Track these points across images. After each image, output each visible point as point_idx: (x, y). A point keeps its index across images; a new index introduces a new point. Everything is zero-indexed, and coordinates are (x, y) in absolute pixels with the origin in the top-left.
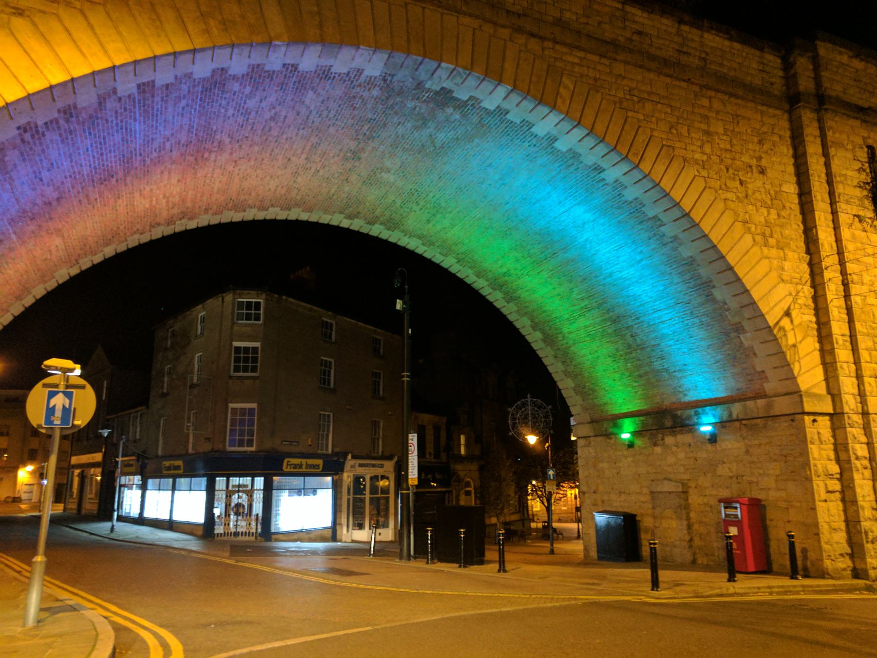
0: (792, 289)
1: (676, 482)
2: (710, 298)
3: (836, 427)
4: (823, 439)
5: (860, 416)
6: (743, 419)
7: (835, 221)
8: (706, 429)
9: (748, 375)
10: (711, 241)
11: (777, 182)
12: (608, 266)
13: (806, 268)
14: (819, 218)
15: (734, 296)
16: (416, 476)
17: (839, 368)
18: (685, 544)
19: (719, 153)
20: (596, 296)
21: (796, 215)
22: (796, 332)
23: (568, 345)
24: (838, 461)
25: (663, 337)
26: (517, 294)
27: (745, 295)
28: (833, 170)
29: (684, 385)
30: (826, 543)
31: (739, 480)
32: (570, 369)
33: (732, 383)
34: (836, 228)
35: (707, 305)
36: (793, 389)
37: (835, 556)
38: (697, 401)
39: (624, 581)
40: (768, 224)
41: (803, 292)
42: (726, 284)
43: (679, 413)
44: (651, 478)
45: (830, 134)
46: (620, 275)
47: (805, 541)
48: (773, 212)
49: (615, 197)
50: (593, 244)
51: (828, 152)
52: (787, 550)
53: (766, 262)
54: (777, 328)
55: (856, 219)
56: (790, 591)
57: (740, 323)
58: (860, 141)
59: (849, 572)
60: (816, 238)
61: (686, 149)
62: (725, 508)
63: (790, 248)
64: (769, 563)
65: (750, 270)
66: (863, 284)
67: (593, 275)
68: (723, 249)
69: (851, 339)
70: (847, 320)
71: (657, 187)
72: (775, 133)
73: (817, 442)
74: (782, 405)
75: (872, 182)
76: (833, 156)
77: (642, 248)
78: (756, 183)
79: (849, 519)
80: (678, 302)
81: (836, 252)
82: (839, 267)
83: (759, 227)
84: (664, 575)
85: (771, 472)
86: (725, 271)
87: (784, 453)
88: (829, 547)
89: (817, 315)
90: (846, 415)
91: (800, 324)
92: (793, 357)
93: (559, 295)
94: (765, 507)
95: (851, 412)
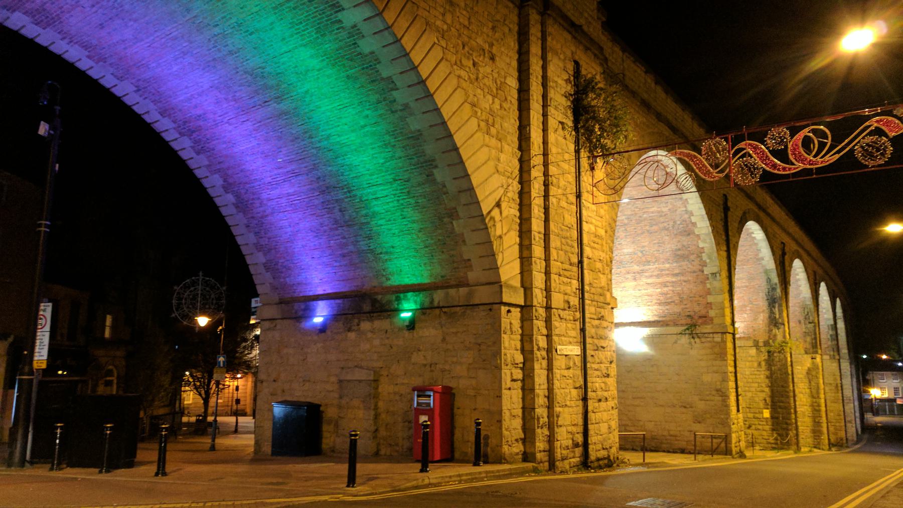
0: (504, 181)
1: (368, 369)
4: (514, 329)
5: (544, 309)
12: (327, 127)
14: (533, 117)
15: (455, 179)
16: (45, 357)
19: (458, 27)
20: (307, 160)
21: (514, 110)
24: (523, 351)
25: (374, 214)
28: (548, 75)
29: (388, 268)
30: (506, 430)
31: (432, 368)
32: (263, 242)
33: (438, 270)
34: (545, 130)
37: (511, 441)
40: (491, 113)
41: (513, 186)
43: (379, 297)
44: (342, 366)
45: (549, 39)
46: (338, 139)
49: (350, 46)
50: (314, 97)
52: (472, 438)
53: (485, 149)
56: (476, 478)
57: (455, 208)
58: (569, 53)
61: (429, 12)
62: (419, 396)
63: (506, 141)
65: (473, 154)
66: (559, 187)
69: (545, 237)
70: (543, 219)
73: (509, 332)
74: (482, 295)
75: (574, 94)
78: (486, 69)
79: (526, 406)
80: (397, 178)
83: (484, 113)
84: (362, 468)
87: (479, 341)
89: (520, 210)
91: (507, 217)
92: (498, 247)
94: (454, 394)
95: (538, 305)
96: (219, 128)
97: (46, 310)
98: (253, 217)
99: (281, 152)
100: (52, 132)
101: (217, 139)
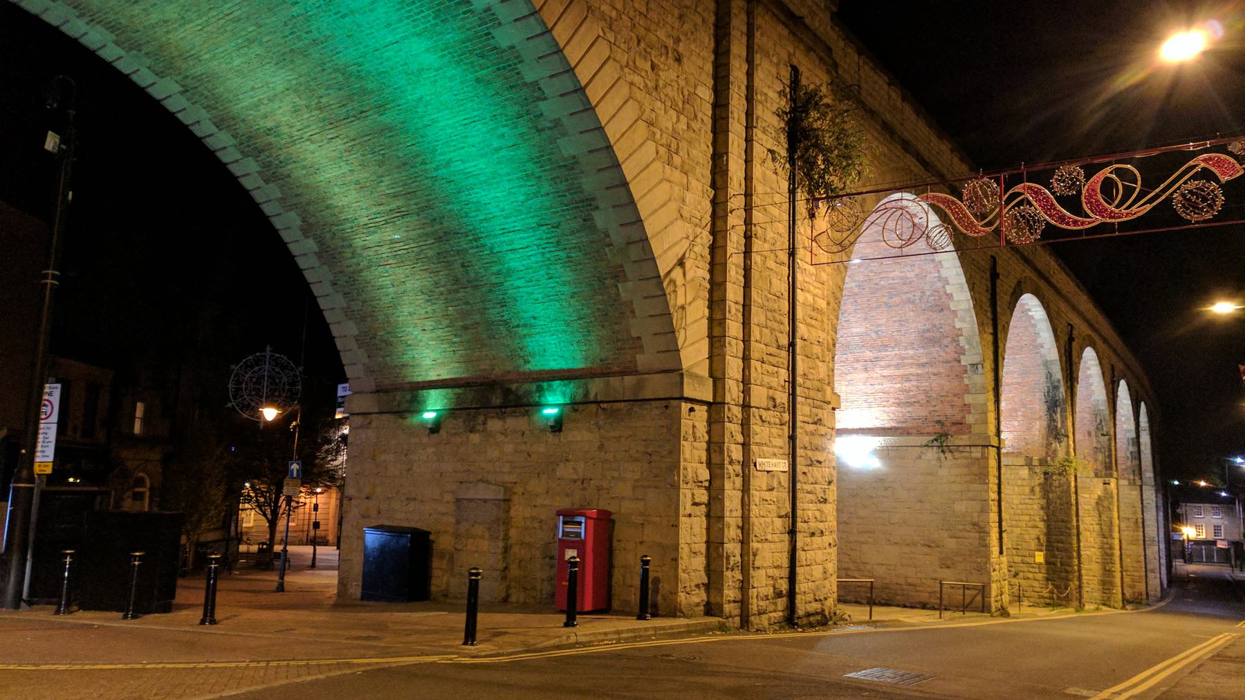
0: (690, 231)
2: (588, 224)
3: (712, 420)
4: (698, 435)
7: (749, 150)
8: (550, 412)
10: (606, 139)
12: (446, 150)
13: (708, 207)
15: (622, 225)
18: (496, 574)
19: (632, 14)
23: (360, 268)
24: (709, 464)
25: (510, 272)
26: (285, 171)
30: (684, 571)
31: (585, 485)
34: (748, 161)
35: (583, 234)
37: (690, 587)
38: (541, 372)
39: (417, 632)
43: (514, 387)
45: (758, 34)
47: (659, 569)
48: (683, 119)
49: (481, 36)
50: (429, 107)
51: (753, 58)
52: (637, 581)
53: (666, 185)
54: (667, 280)
55: (770, 155)
57: (622, 266)
58: (785, 57)
59: (702, 608)
60: (725, 168)
62: (565, 523)
67: (419, 160)
71: (548, 34)
72: (699, 13)
73: (691, 438)
74: (656, 386)
75: (790, 112)
76: (757, 65)
77: (505, 130)
80: (542, 222)
81: (743, 193)
83: (664, 135)
85: (629, 475)
86: (617, 186)
87: (650, 450)
89: (711, 272)
92: (679, 323)
93: (358, 182)
94: (613, 522)
95: (732, 402)
96: (298, 146)
97: (53, 394)
98: (341, 272)
99: (382, 182)
100: (64, 147)
101: (295, 162)
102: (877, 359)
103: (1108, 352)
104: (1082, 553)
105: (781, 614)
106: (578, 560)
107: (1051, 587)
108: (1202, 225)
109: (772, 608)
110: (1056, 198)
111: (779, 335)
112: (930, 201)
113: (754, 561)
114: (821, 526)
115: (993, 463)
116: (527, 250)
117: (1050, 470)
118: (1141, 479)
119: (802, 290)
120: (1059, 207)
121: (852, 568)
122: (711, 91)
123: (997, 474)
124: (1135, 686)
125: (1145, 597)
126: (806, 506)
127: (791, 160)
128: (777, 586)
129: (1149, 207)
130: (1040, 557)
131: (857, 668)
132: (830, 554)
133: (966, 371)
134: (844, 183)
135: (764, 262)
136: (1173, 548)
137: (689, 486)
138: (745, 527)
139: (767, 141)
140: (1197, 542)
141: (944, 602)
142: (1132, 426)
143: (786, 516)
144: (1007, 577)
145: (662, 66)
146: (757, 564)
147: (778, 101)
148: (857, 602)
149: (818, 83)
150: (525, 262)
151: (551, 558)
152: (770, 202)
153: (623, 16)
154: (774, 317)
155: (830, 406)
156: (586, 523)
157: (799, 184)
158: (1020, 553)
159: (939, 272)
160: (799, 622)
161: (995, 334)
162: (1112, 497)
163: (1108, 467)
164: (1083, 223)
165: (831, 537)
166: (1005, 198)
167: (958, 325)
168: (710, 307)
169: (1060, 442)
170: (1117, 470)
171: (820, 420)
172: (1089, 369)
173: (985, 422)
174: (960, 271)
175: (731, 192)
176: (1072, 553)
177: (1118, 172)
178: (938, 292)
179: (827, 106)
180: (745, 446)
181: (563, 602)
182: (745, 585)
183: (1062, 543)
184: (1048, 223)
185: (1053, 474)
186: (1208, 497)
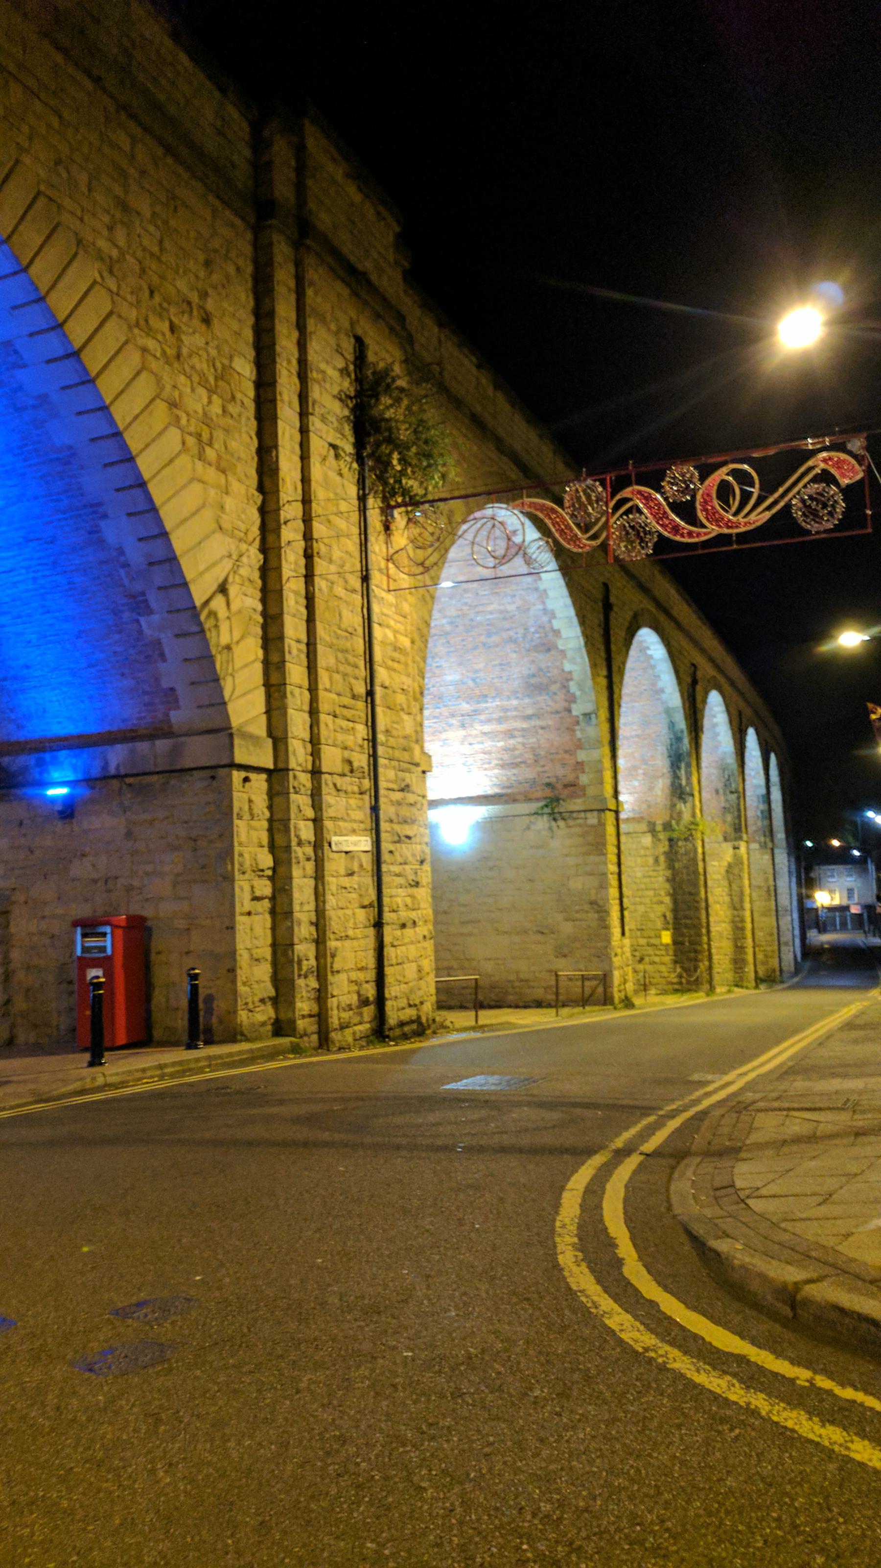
0: (233, 547)
4: (256, 811)
6: (127, 776)
9: (145, 693)
10: (112, 422)
11: (226, 349)
17: (288, 695)
19: (139, 254)
21: (248, 419)
22: (234, 625)
24: (272, 847)
27: (159, 541)
28: (310, 358)
30: (244, 984)
34: (305, 457)
36: (217, 724)
38: (42, 741)
41: (249, 557)
42: (129, 515)
45: (310, 292)
52: (184, 1002)
53: (197, 487)
55: (332, 452)
56: (190, 1070)
57: (143, 594)
58: (346, 324)
59: (269, 1028)
62: (84, 935)
63: (235, 474)
64: (148, 1027)
65: (174, 495)
68: (134, 442)
70: (305, 617)
71: (23, 275)
73: (247, 816)
75: (355, 397)
76: (311, 333)
80: (31, 536)
81: (300, 498)
82: (301, 526)
83: (193, 421)
85: (166, 869)
86: (131, 487)
87: (194, 834)
88: (247, 989)
89: (264, 601)
90: (291, 773)
91: (240, 612)
94: (149, 930)
95: (299, 768)
102: (476, 712)
103: (735, 697)
104: (712, 929)
105: (368, 1026)
106: (103, 980)
107: (679, 970)
108: (824, 536)
109: (356, 1019)
110: (669, 504)
111: (353, 681)
112: (527, 509)
113: (332, 963)
114: (413, 915)
115: (610, 830)
116: (12, 574)
117: (675, 835)
118: (772, 841)
119: (380, 624)
120: (673, 516)
121: (455, 967)
122: (252, 365)
123: (615, 842)
124: (762, 1065)
125: (778, 973)
126: (394, 891)
127: (359, 458)
128: (362, 992)
129: (768, 515)
130: (666, 937)
131: (458, 1078)
132: (425, 948)
133: (578, 723)
134: (426, 489)
135: (331, 589)
136: (806, 917)
137: (247, 876)
138: (320, 922)
139: (327, 432)
140: (832, 909)
141: (561, 998)
142: (762, 781)
143: (371, 905)
144: (630, 962)
145: (184, 328)
146: (336, 967)
147: (339, 380)
148: (463, 1007)
149: (390, 361)
150: (9, 592)
151: (70, 982)
152: (335, 510)
153: (128, 257)
154: (346, 660)
155: (420, 769)
156: (112, 933)
157: (370, 490)
158: (645, 934)
159: (544, 603)
160: (391, 1034)
161: (609, 677)
162: (742, 863)
163: (738, 829)
164: (699, 535)
165: (426, 928)
166: (612, 504)
167: (568, 667)
168: (265, 647)
169: (685, 802)
170: (747, 833)
171: (408, 786)
172: (715, 716)
173: (601, 782)
174: (568, 601)
175: (284, 497)
176: (700, 929)
177: (734, 473)
178: (544, 628)
179: (402, 390)
180: (317, 822)
181: (87, 1039)
182: (323, 994)
183: (691, 918)
184: (660, 535)
185: (679, 839)
186: (841, 858)
